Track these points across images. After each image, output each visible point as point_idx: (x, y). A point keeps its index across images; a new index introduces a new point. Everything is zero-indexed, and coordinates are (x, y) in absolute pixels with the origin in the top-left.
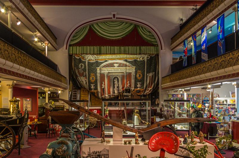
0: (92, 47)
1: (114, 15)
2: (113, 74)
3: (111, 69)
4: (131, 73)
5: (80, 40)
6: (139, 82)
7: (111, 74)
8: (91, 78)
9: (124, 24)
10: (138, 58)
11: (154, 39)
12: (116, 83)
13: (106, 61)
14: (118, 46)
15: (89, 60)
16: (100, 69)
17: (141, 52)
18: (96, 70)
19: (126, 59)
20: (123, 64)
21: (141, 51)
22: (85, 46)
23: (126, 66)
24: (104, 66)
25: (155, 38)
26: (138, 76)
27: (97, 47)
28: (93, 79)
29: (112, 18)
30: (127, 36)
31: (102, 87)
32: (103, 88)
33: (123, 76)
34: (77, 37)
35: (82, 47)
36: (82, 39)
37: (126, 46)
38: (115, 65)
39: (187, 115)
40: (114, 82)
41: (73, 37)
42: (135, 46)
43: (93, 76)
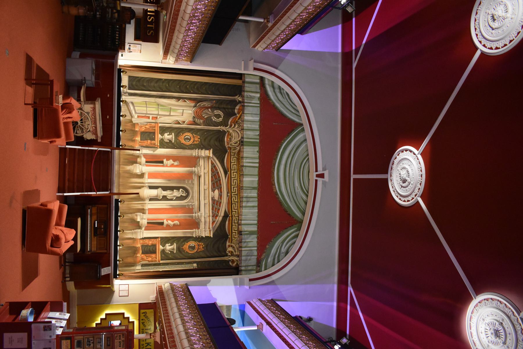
0: (257, 126)
1: (322, 176)
3: (207, 182)
4: (198, 228)
5: (273, 102)
6: (178, 249)
9: (304, 197)
10: (232, 242)
11: (271, 263)
12: (176, 193)
13: (226, 173)
15: (230, 134)
16: (209, 157)
19: (230, 215)
20: (219, 210)
21: (247, 234)
23: (213, 216)
24: (215, 167)
25: (273, 265)
26: (192, 243)
28: (185, 139)
29: (316, 171)
30: (280, 203)
31: (167, 160)
32: (165, 160)
34: (279, 95)
37: (259, 201)
38: (217, 192)
40: (178, 188)
41: (280, 87)
42: (258, 221)
43: (194, 141)
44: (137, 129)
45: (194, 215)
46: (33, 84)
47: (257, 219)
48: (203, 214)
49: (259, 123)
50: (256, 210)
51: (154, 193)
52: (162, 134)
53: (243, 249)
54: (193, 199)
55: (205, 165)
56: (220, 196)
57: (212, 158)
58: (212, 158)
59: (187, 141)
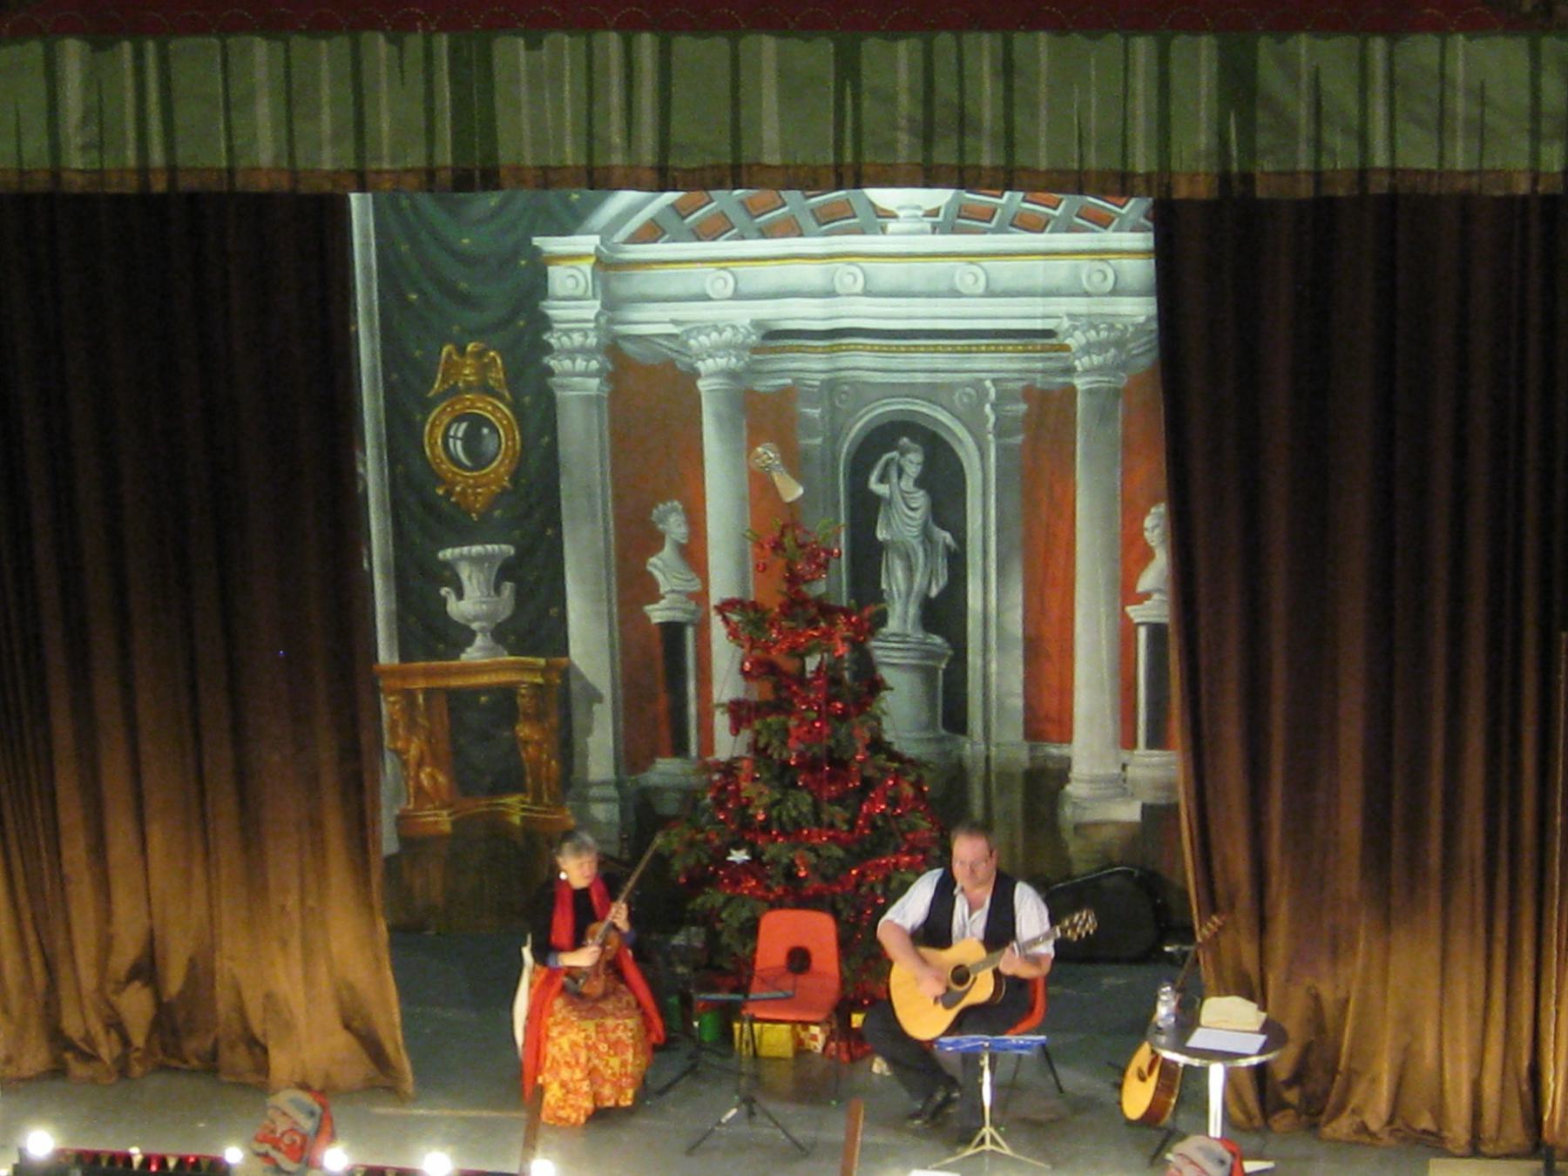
2: (862, 362)
3: (811, 274)
7: (813, 365)
8: (442, 437)
14: (810, 26)
16: (606, 265)
17: (1250, 152)
18: (537, 286)
21: (1248, 128)
22: (200, 29)
27: (414, 42)
28: (479, 460)
31: (651, 592)
32: (658, 613)
33: (1044, 419)
35: (150, 46)
37: (958, 25)
40: (865, 509)
42: (1135, 24)
43: (488, 390)
44: (442, 821)
45: (1080, 383)
47: (1114, 40)
48: (1080, 305)
49: (298, 42)
50: (1040, 49)
52: (461, 636)
53: (1380, 159)
54: (951, 387)
55: (675, 288)
57: (607, 232)
58: (607, 232)
59: (490, 445)
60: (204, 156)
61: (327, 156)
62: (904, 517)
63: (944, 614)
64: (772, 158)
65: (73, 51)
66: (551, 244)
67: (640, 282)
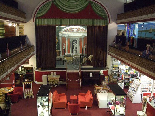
3: (71, 33)
7: (70, 37)
14: (76, 19)
16: (62, 33)
20: (81, 29)
21: (93, 24)
22: (49, 18)
24: (65, 30)
25: (105, 13)
27: (58, 19)
31: (63, 47)
32: (64, 48)
33: (81, 39)
35: (47, 19)
36: (46, 13)
39: (124, 87)
40: (73, 44)
41: (39, 11)
46: (103, 90)
47: (88, 19)
51: (74, 52)
56: (76, 28)
57: (62, 32)
60: (49, 24)
61: (54, 24)
62: (75, 44)
63: (76, 48)
64: (74, 24)
65: (43, 19)
66: (59, 32)
67: (63, 34)
